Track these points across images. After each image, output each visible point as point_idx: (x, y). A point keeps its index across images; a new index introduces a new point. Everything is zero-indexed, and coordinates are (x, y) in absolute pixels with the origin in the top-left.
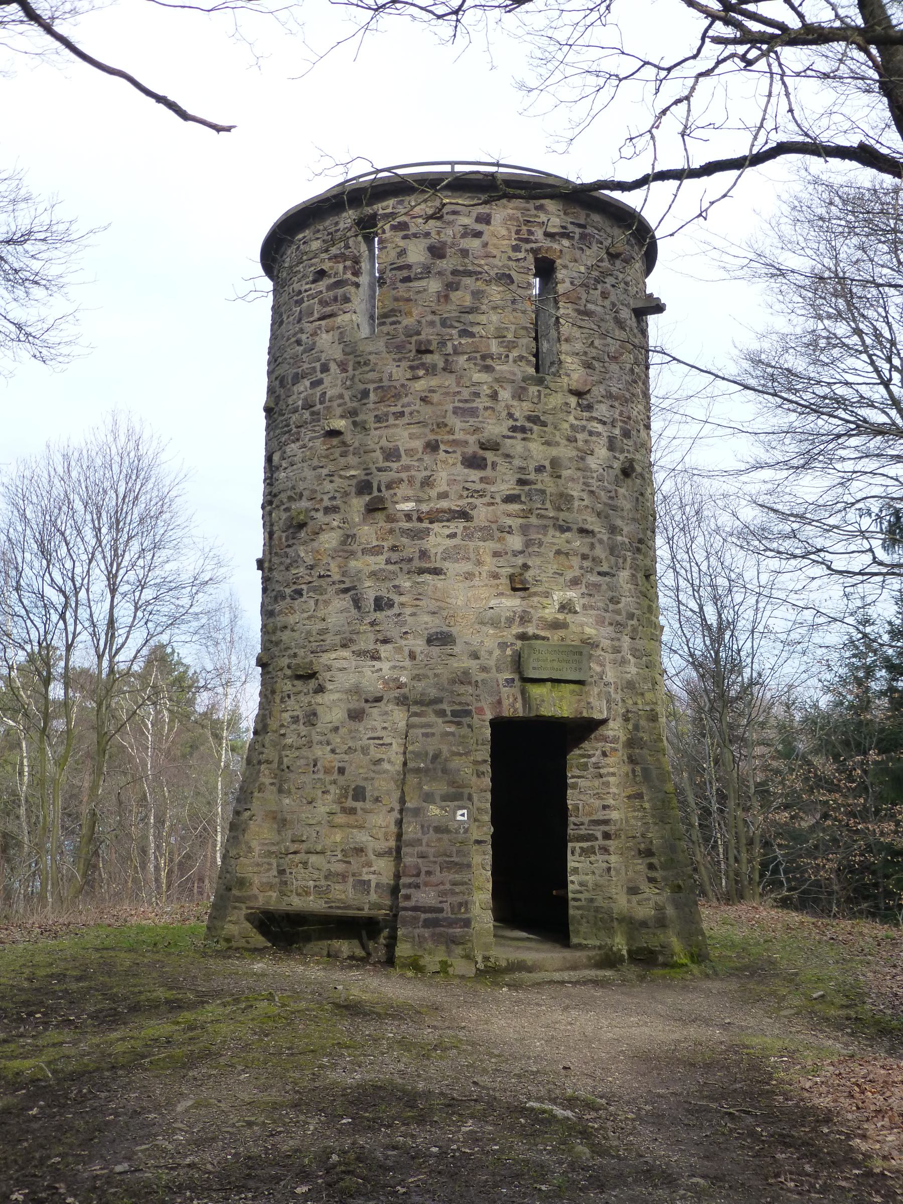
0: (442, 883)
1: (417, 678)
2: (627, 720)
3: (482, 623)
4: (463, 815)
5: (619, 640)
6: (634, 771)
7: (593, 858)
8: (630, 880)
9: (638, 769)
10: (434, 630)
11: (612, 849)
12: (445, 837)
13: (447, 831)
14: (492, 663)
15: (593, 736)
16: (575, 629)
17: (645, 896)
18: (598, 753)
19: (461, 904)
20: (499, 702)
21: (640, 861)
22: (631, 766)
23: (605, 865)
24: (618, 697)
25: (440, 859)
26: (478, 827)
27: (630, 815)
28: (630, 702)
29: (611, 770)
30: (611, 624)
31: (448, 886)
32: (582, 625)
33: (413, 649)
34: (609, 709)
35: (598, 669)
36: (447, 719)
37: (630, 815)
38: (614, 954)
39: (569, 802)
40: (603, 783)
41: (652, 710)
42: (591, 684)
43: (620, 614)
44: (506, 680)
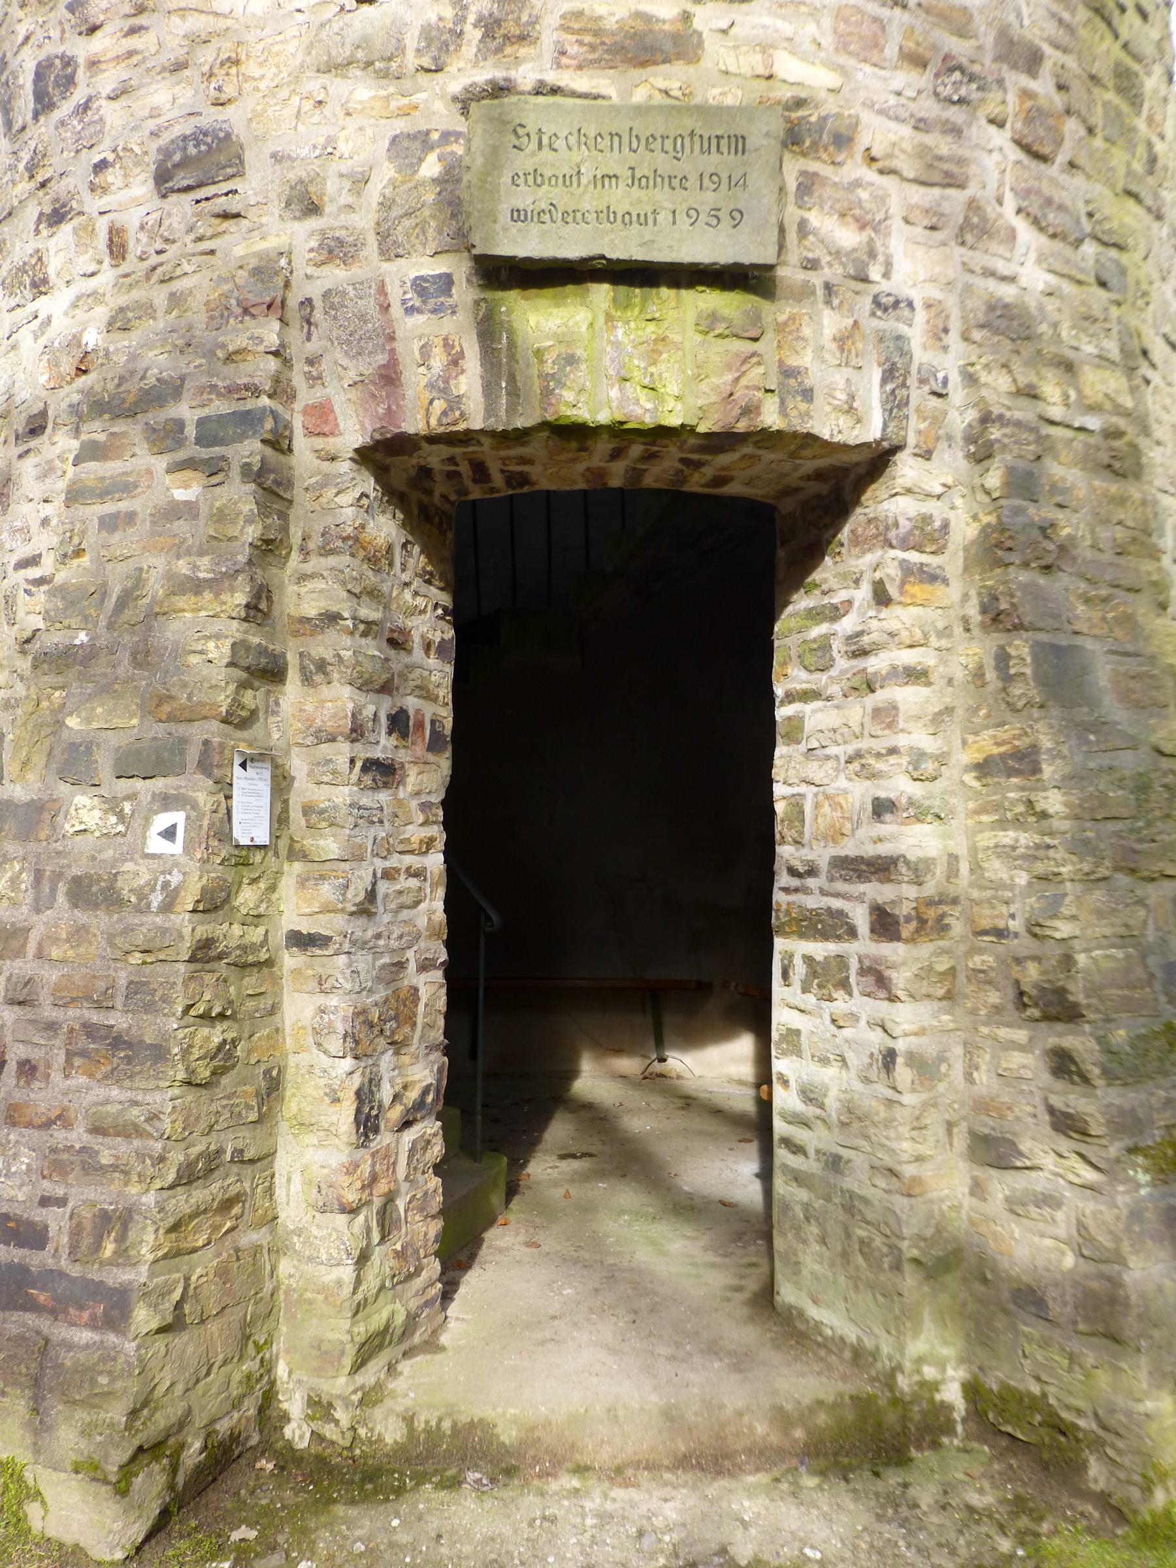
0: (62, 1119)
1: (119, 323)
2: (982, 455)
3: (333, 67)
4: (169, 834)
5: (956, 131)
6: (1003, 659)
7: (841, 1004)
8: (982, 1106)
9: (1021, 648)
10: (177, 131)
11: (900, 979)
12: (100, 921)
13: (111, 899)
14: (364, 220)
15: (845, 534)
16: (730, 62)
17: (1038, 1182)
18: (863, 593)
19: (104, 1219)
20: (389, 377)
21: (1021, 1035)
22: (997, 639)
23: (876, 1039)
24: (949, 365)
25: (73, 1015)
26: (303, 882)
27: (987, 839)
28: (1003, 382)
29: (908, 657)
30: (920, 62)
31: (78, 1136)
32: (765, 48)
33: (119, 218)
34: (895, 405)
35: (848, 237)
36: (182, 455)
37: (987, 839)
38: (897, 1401)
39: (778, 790)
40: (877, 712)
41: (1112, 434)
42: (805, 292)
43: (963, 32)
44: (420, 286)
